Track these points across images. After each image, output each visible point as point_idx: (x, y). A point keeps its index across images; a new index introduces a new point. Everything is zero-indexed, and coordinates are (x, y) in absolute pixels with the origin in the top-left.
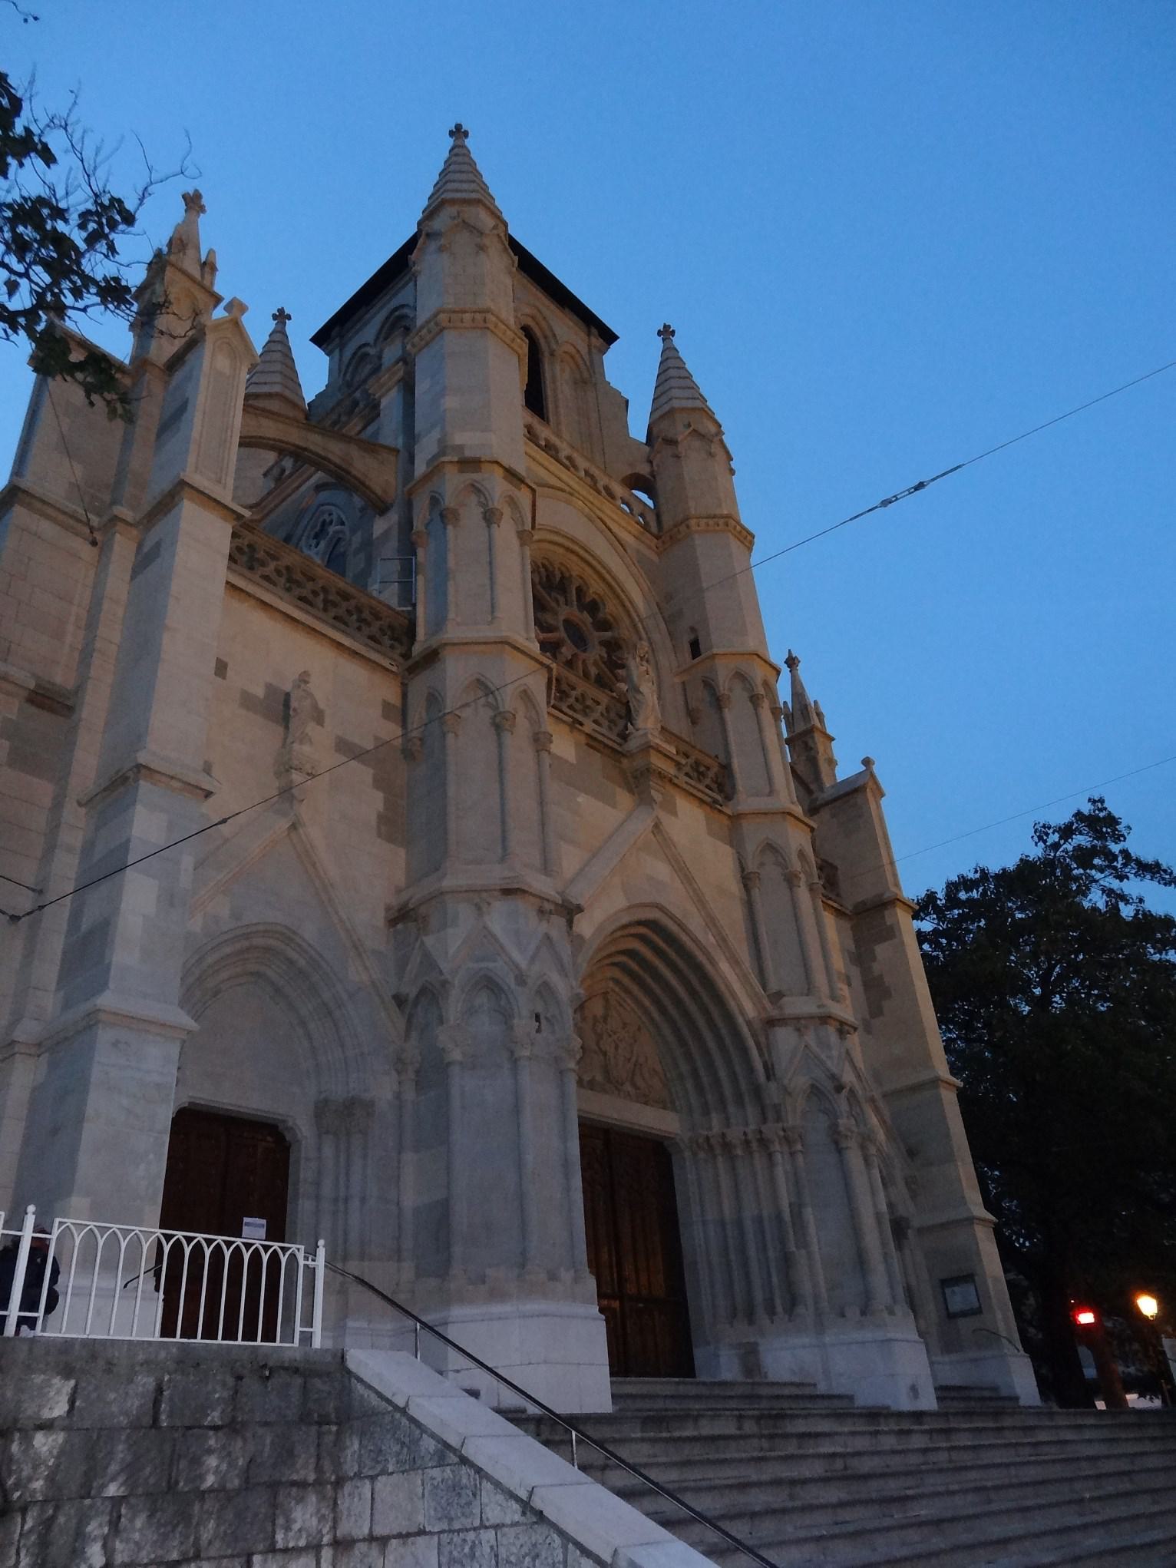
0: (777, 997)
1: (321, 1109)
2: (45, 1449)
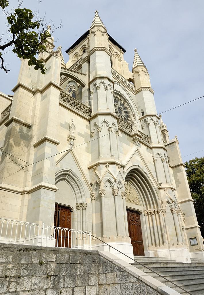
0: (160, 184)
2: (53, 266)
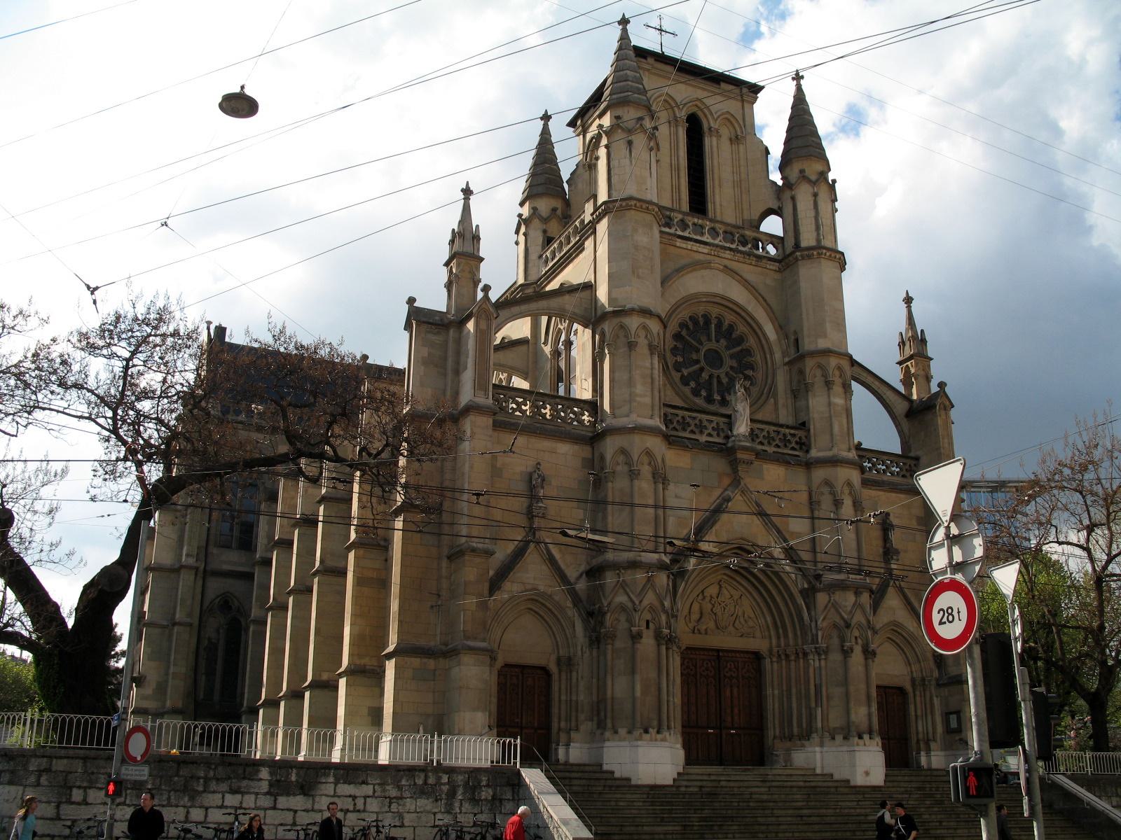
1: (559, 661)
